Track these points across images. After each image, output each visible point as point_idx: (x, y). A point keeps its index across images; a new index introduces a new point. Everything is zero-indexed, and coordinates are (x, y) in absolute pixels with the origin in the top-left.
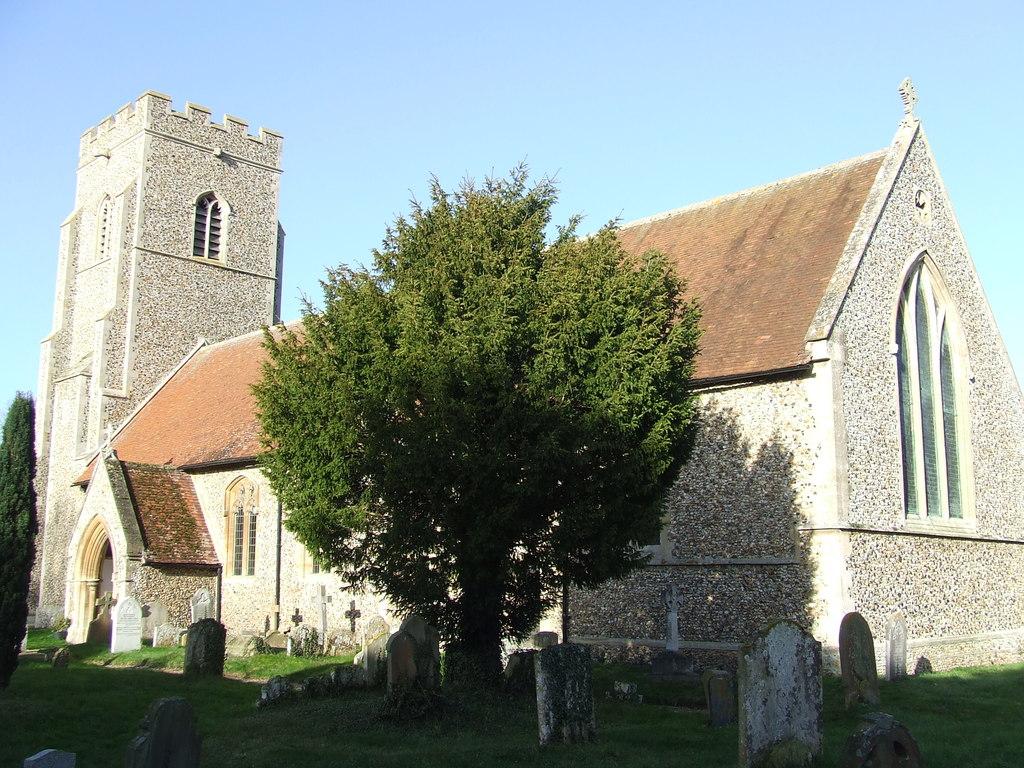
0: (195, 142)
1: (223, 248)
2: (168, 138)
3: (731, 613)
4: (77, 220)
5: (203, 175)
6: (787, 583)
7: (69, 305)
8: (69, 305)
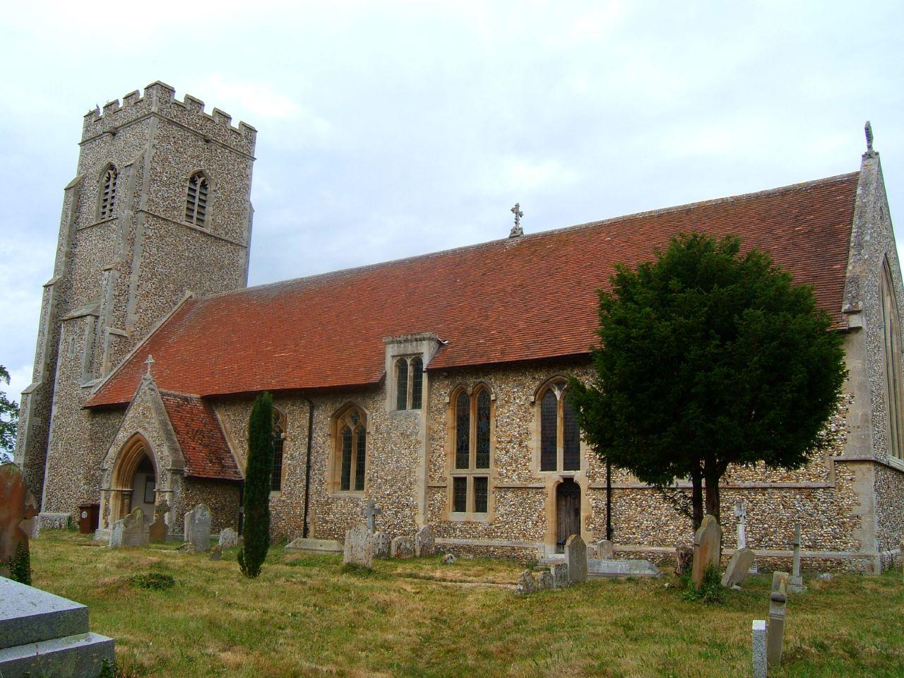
0: (191, 128)
1: (208, 218)
2: (170, 122)
3: (770, 527)
5: (192, 159)
6: (824, 502)
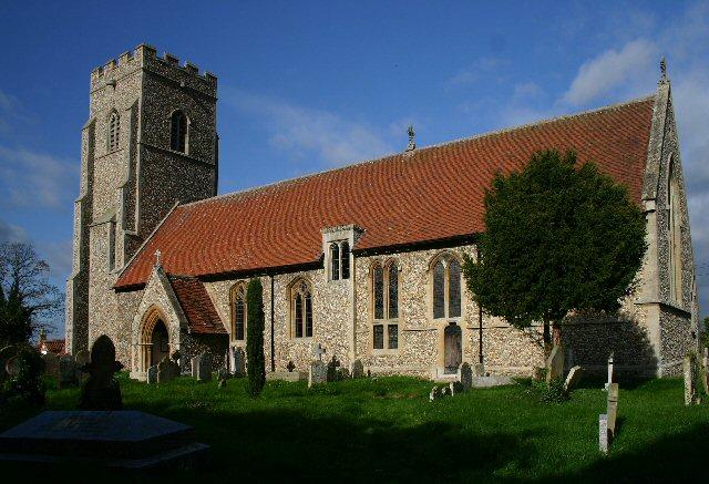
4: (92, 127)
7: (91, 178)
8: (91, 178)
